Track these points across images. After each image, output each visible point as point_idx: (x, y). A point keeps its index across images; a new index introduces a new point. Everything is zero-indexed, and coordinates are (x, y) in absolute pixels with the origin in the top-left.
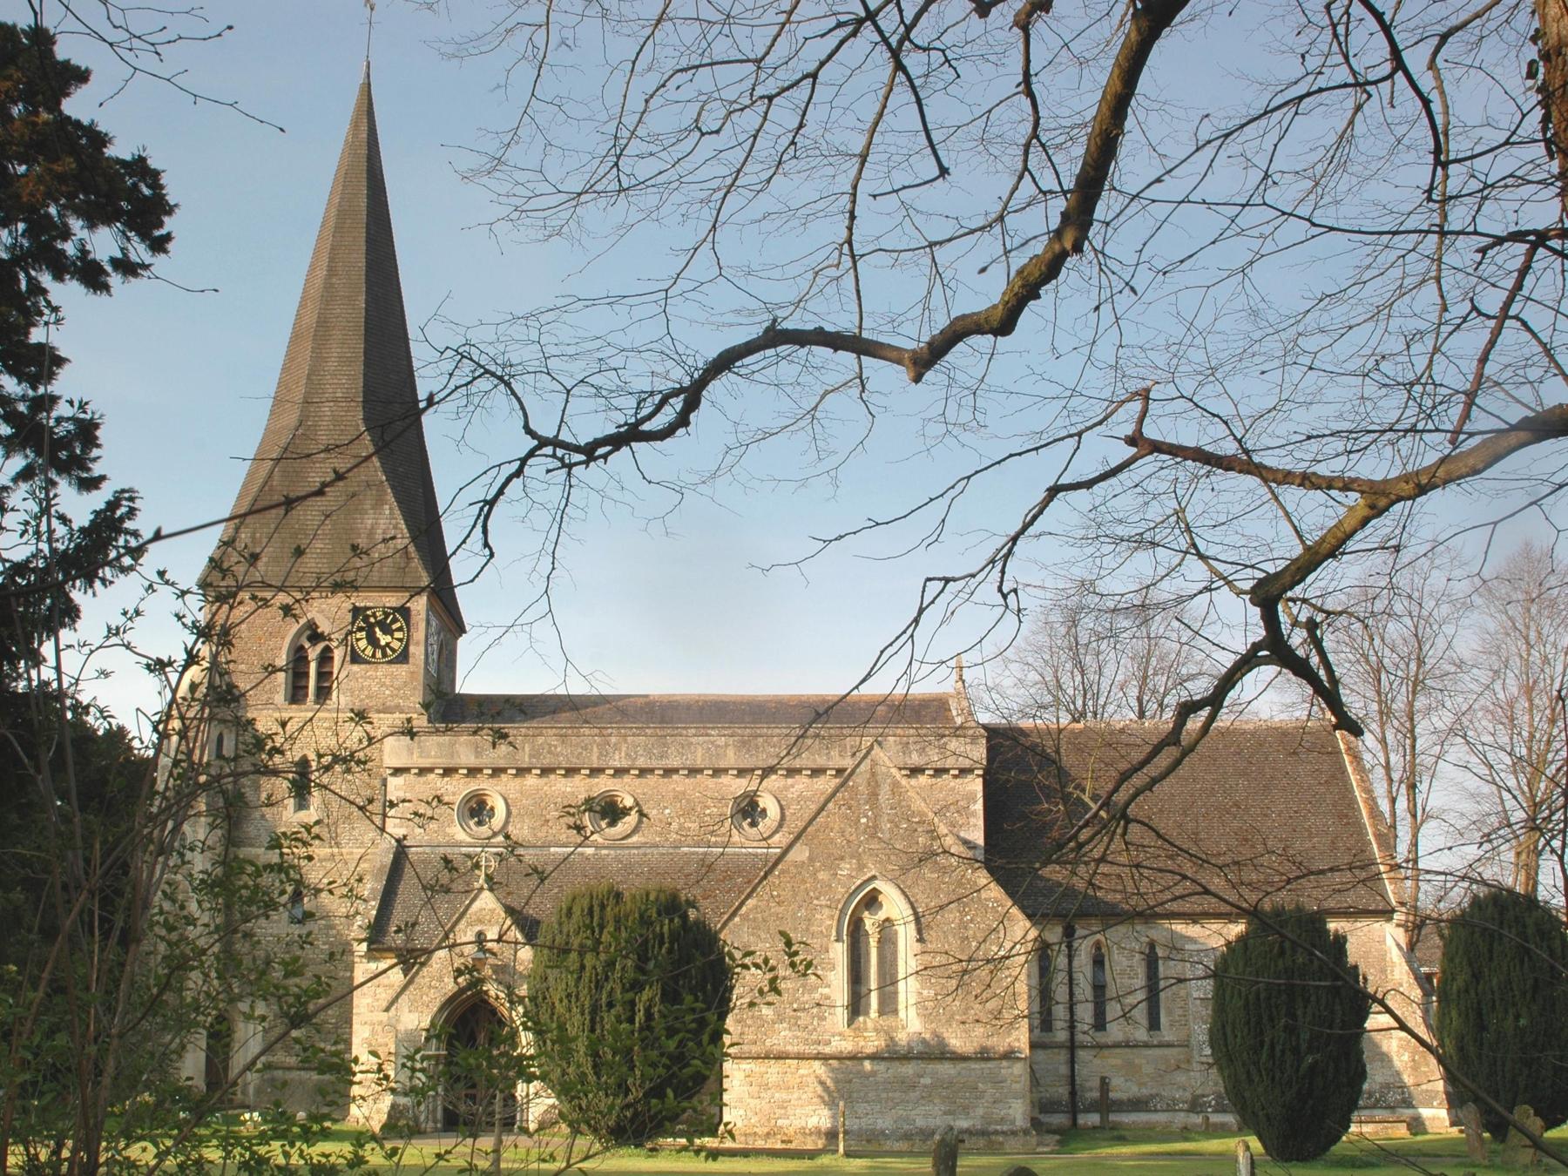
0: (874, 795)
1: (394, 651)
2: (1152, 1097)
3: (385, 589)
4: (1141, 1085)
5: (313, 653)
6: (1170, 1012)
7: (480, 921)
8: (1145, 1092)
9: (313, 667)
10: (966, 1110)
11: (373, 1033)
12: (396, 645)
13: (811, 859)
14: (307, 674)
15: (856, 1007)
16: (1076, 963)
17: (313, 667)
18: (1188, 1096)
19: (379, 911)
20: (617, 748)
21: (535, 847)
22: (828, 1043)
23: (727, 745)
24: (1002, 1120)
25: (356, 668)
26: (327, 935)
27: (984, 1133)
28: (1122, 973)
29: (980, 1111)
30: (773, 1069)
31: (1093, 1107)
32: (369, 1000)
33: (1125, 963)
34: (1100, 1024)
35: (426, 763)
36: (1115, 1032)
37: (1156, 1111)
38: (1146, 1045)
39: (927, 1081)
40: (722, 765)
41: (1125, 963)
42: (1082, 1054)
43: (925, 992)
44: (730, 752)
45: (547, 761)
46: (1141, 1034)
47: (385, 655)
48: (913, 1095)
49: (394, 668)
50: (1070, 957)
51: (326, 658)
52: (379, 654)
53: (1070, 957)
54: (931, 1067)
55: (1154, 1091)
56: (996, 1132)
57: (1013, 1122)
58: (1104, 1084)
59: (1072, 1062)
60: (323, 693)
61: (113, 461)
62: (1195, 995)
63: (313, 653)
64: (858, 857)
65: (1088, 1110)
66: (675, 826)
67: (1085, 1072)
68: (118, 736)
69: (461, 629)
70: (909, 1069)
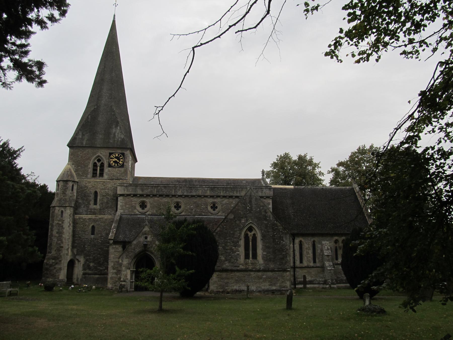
0: (250, 202)
1: (120, 164)
2: (314, 280)
3: (118, 148)
4: (311, 277)
5: (99, 164)
6: (318, 259)
7: (146, 234)
8: (312, 279)
9: (98, 168)
10: (274, 284)
11: (114, 264)
12: (121, 162)
13: (234, 218)
14: (97, 170)
15: (247, 257)
16: (295, 245)
17: (98, 168)
18: (323, 279)
19: (116, 231)
20: (179, 190)
21: (157, 215)
22: (239, 267)
23: (207, 190)
24: (284, 287)
25: (110, 168)
26: (101, 238)
27: (279, 291)
28: (307, 249)
29: (278, 285)
30: (224, 275)
31: (300, 283)
32: (113, 256)
33: (307, 246)
34: (301, 262)
35: (128, 193)
36: (305, 264)
37: (315, 284)
38: (313, 267)
39: (264, 277)
40: (206, 195)
41: (307, 246)
42: (297, 269)
43: (264, 253)
44: (208, 192)
45: (161, 193)
46: (312, 264)
47: (118, 165)
48: (261, 280)
49: (120, 169)
50: (294, 244)
51: (102, 165)
52: (116, 165)
53: (294, 244)
54: (265, 273)
55: (315, 279)
56: (283, 290)
57: (287, 287)
58: (305, 277)
59: (294, 271)
60: (101, 175)
61: (63, 19)
62: (325, 254)
63: (99, 164)
64: (246, 217)
65: (298, 284)
66: (194, 210)
67: (297, 274)
68: (44, 187)
69: (136, 161)
70: (260, 274)
